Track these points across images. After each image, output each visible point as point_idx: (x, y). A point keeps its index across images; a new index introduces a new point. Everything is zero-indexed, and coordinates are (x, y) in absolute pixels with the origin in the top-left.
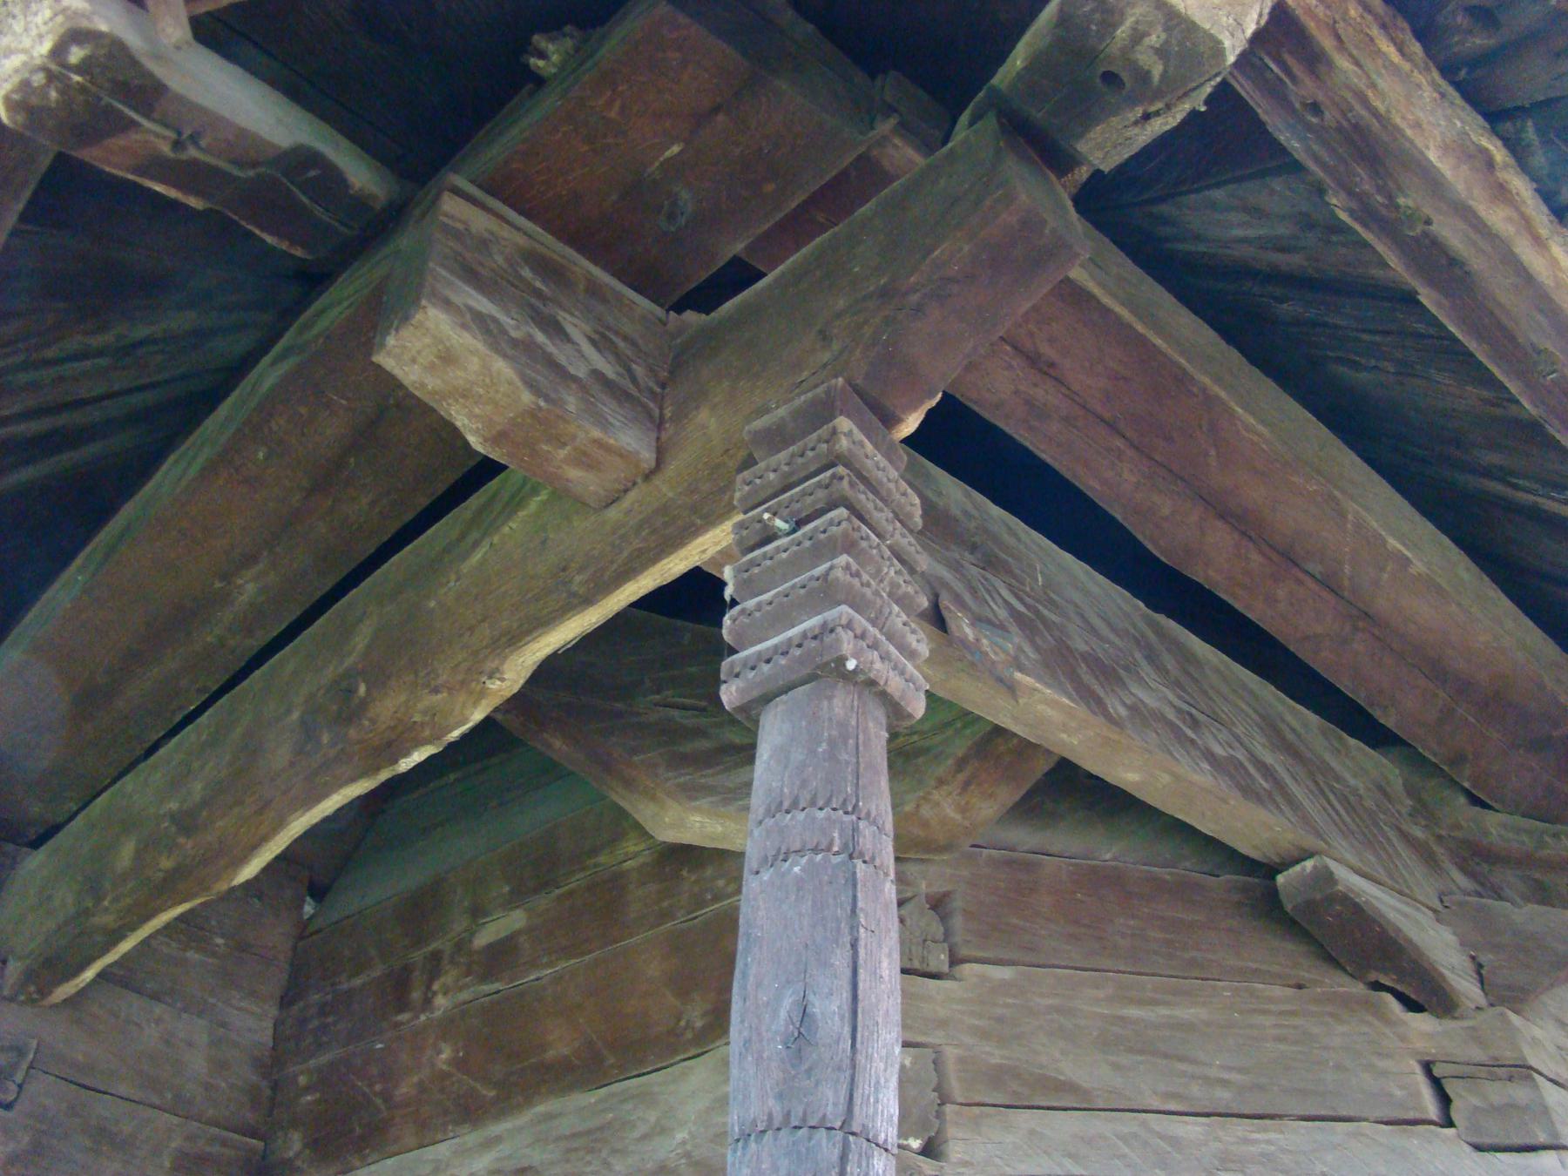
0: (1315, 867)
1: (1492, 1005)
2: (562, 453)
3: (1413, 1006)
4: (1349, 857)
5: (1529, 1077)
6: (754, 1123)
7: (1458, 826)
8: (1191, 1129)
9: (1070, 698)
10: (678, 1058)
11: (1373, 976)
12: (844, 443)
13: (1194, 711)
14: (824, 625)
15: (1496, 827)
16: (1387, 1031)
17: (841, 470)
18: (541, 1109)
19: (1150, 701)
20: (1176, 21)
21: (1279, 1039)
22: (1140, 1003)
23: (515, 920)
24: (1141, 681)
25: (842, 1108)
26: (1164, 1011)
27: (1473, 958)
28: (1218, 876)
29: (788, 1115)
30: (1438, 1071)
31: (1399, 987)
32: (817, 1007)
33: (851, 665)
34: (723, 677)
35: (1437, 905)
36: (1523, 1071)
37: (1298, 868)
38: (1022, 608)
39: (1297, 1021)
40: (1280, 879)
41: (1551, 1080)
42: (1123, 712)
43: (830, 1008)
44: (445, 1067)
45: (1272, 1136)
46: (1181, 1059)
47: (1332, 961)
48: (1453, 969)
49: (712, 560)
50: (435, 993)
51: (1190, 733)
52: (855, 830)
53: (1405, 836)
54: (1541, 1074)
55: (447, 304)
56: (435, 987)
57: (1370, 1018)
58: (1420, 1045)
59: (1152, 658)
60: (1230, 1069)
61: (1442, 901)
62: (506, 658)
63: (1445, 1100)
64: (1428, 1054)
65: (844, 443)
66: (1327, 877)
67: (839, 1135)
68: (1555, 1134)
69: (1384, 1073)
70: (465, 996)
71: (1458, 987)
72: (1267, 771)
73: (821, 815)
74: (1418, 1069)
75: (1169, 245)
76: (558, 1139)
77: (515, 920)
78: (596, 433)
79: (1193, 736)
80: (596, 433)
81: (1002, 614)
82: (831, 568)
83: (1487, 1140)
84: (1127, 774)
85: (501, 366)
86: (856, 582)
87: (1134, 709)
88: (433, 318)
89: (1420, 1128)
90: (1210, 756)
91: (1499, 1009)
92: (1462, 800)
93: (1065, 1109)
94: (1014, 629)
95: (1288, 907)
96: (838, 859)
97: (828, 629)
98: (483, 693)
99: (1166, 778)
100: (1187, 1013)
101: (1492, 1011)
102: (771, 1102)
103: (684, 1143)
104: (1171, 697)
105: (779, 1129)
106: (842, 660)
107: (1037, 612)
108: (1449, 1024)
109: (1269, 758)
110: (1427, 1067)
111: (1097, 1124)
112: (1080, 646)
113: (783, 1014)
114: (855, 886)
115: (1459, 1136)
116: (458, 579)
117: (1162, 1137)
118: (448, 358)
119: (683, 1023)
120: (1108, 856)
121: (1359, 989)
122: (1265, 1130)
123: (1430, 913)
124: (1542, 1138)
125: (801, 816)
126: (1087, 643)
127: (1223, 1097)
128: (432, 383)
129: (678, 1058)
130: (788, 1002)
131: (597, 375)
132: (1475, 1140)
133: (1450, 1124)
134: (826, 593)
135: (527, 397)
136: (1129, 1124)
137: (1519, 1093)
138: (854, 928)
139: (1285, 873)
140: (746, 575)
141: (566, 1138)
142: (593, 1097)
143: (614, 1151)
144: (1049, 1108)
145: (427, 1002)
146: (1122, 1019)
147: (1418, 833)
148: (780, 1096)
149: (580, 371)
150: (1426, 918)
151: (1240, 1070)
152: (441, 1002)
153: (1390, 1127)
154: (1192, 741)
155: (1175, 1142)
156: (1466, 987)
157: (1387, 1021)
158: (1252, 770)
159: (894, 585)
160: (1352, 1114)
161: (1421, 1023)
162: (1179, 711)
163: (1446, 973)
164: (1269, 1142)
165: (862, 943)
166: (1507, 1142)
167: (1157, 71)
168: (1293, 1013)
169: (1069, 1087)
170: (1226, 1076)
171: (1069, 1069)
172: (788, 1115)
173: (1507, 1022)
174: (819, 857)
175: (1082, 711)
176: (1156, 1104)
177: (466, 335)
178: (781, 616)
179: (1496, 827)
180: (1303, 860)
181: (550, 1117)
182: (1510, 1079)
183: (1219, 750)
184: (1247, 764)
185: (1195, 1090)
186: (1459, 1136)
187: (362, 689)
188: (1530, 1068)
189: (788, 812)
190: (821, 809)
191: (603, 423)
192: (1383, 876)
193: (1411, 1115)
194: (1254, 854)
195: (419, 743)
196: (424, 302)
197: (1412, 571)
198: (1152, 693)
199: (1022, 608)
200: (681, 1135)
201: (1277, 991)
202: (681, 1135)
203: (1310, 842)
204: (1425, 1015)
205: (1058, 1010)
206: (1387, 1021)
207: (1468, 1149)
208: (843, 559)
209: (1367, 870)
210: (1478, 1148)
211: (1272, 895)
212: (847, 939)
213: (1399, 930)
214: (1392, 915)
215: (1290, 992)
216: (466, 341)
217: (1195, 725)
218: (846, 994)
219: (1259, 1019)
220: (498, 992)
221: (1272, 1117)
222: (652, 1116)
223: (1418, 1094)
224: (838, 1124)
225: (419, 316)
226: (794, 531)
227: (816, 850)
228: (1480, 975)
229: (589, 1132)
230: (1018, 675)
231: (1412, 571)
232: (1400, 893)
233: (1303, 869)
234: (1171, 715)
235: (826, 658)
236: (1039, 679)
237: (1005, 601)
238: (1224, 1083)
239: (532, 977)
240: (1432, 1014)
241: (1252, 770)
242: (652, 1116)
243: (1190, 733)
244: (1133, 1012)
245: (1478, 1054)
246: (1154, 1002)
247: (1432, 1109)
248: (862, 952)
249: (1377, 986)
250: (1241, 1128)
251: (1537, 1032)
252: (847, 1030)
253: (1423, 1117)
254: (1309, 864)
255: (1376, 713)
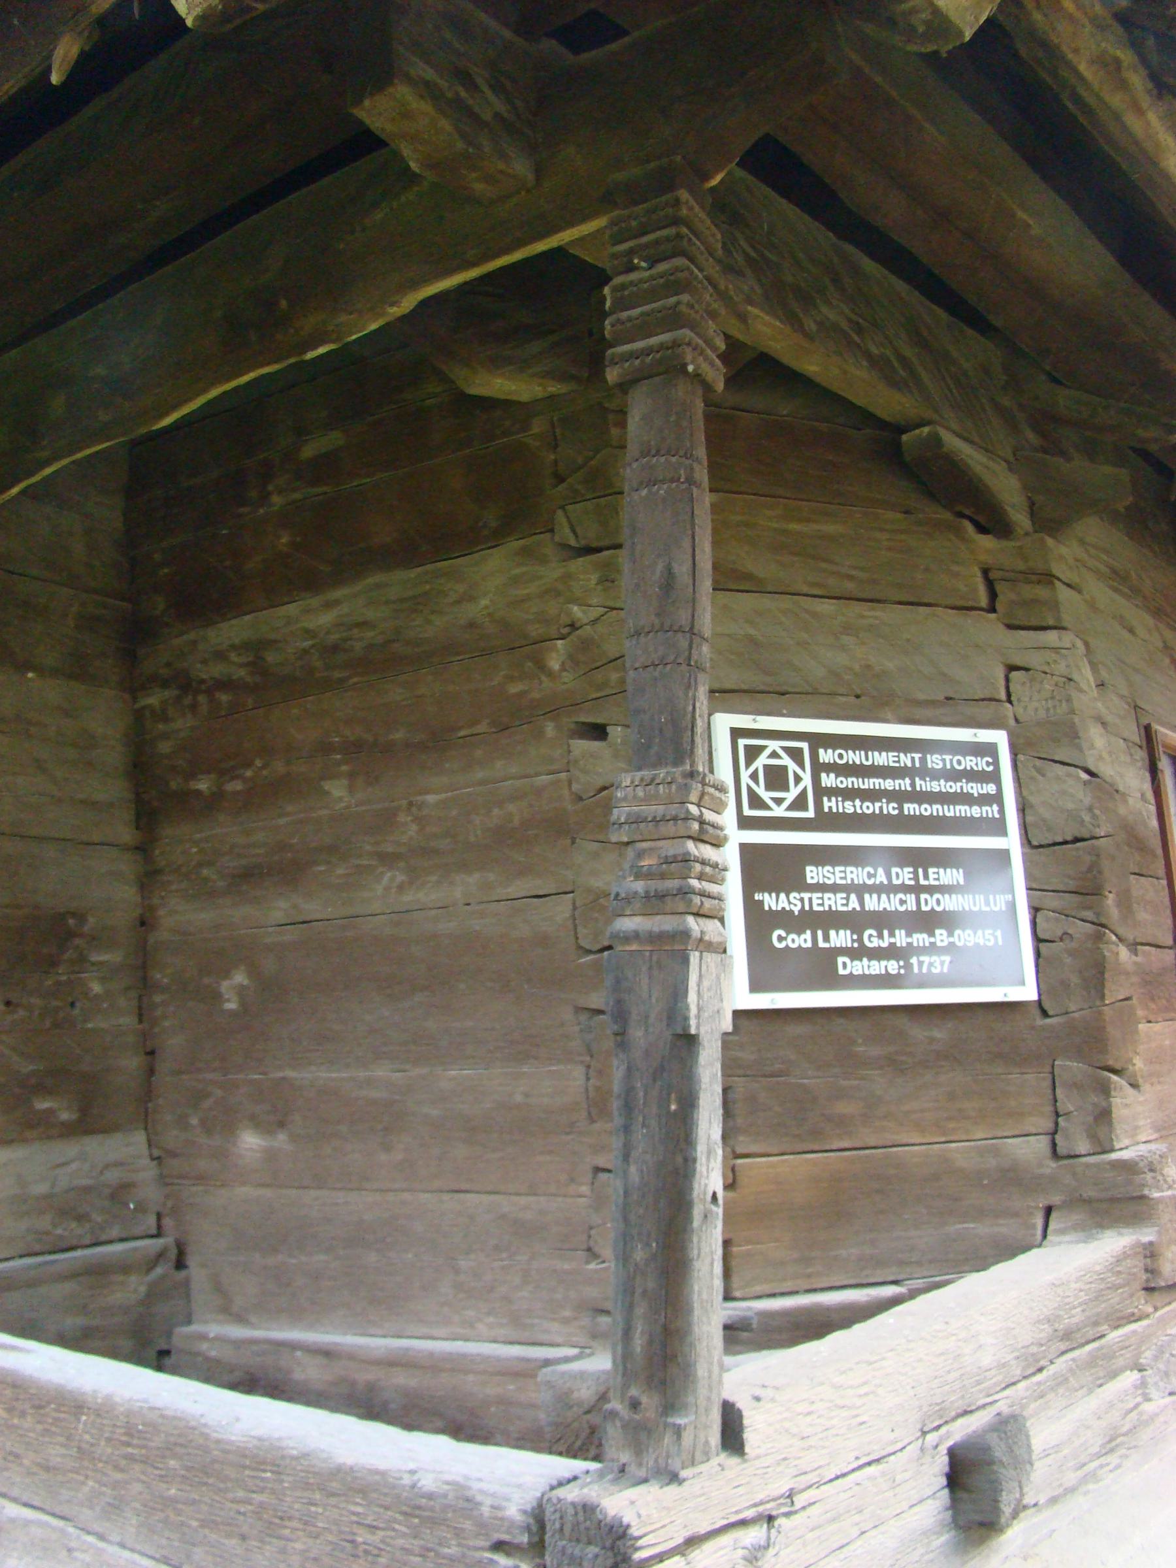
0: (929, 433)
1: (1036, 532)
2: (474, 175)
3: (982, 529)
4: (954, 426)
5: (1052, 583)
6: (643, 628)
7: (1037, 398)
8: (826, 607)
9: (781, 322)
10: (479, 548)
11: (959, 508)
12: (684, 212)
13: (861, 321)
14: (674, 341)
15: (1064, 399)
16: (963, 547)
17: (685, 230)
18: (370, 581)
19: (832, 316)
20: (936, 11)
21: (889, 549)
22: (800, 520)
23: (334, 439)
24: (828, 303)
25: (689, 621)
26: (815, 527)
27: (1029, 498)
28: (859, 429)
29: (662, 624)
30: (992, 575)
31: (976, 517)
32: (676, 568)
33: (690, 368)
34: (607, 363)
35: (1011, 459)
36: (1048, 578)
37: (917, 431)
38: (753, 254)
39: (903, 537)
40: (905, 437)
41: (1065, 583)
42: (814, 327)
43: (682, 570)
44: (285, 549)
45: (878, 614)
46: (824, 560)
47: (931, 496)
48: (1013, 506)
49: (567, 244)
50: (270, 493)
51: (856, 338)
52: (692, 469)
53: (998, 407)
54: (1059, 579)
55: (409, 80)
56: (270, 488)
57: (952, 537)
58: (983, 557)
59: (836, 281)
60: (855, 568)
61: (1015, 455)
62: (406, 295)
63: (993, 595)
64: (986, 563)
65: (684, 212)
66: (936, 441)
67: (688, 635)
68: (1059, 619)
69: (956, 575)
70: (297, 496)
71: (1014, 519)
72: (903, 360)
73: (674, 459)
74: (979, 574)
75: (1062, 1225)
76: (387, 602)
77: (334, 439)
78: (501, 166)
79: (859, 342)
80: (501, 166)
81: (740, 259)
82: (678, 303)
83: (1017, 622)
84: (811, 367)
85: (445, 124)
86: (692, 312)
87: (820, 324)
88: (402, 91)
89: (973, 613)
90: (869, 356)
91: (1041, 535)
92: (1043, 377)
93: (747, 592)
94: (748, 272)
95: (908, 459)
96: (684, 486)
97: (676, 344)
98: (383, 314)
99: (836, 371)
100: (831, 528)
101: (1037, 535)
102: (653, 617)
103: (486, 607)
104: (847, 311)
105: (657, 632)
106: (685, 365)
107: (762, 255)
108: (1004, 543)
109: (909, 352)
110: (985, 572)
111: (766, 602)
112: (790, 279)
113: (658, 574)
114: (693, 502)
115: (998, 619)
116: (364, 230)
117: (806, 611)
118: (407, 115)
119: (480, 524)
120: (785, 412)
121: (947, 516)
122: (873, 609)
123: (1003, 463)
124: (1051, 622)
125: (663, 459)
126: (794, 275)
127: (849, 586)
128: (389, 127)
129: (479, 548)
130: (660, 567)
131: (497, 115)
132: (1007, 622)
133: (992, 609)
134: (673, 320)
135: (460, 145)
136: (786, 602)
137: (1041, 592)
138: (693, 525)
139: (908, 434)
140: (619, 294)
141: (394, 602)
142: (413, 573)
143: (433, 612)
144: (738, 591)
145: (264, 498)
146: (785, 532)
147: (1006, 402)
148: (658, 615)
149: (487, 116)
150: (1000, 467)
151: (862, 569)
152: (277, 500)
153: (954, 611)
154: (858, 346)
155: (815, 615)
156: (1020, 519)
157: (964, 540)
158: (896, 364)
159: (708, 305)
160: (932, 601)
161: (987, 542)
162: (850, 320)
163: (1009, 509)
164: (876, 618)
165: (696, 534)
166: (1027, 624)
167: (921, 29)
168: (901, 532)
169: (749, 577)
170: (854, 573)
171: (749, 566)
172: (662, 624)
173: (1043, 541)
174: (674, 485)
175: (788, 330)
176: (805, 589)
177: (422, 102)
178: (644, 328)
179: (1064, 399)
180: (924, 425)
181: (378, 586)
182: (1039, 582)
183: (875, 350)
184: (892, 358)
185: (832, 581)
186: (998, 619)
187: (284, 304)
188: (1054, 576)
189: (654, 456)
190: (673, 456)
191: (503, 156)
192: (977, 439)
193: (970, 604)
194: (888, 419)
195: (323, 342)
196: (396, 81)
197: (1033, 232)
198: (834, 312)
199: (753, 254)
200: (484, 602)
201: (890, 515)
202: (484, 602)
203: (928, 414)
204: (990, 537)
205: (747, 525)
206: (964, 540)
207: (1002, 627)
208: (685, 298)
209: (965, 434)
210: (1010, 627)
211: (898, 445)
212: (690, 532)
213: (981, 480)
214: (978, 469)
215: (899, 516)
216: (423, 106)
217: (860, 331)
218: (690, 562)
219: (878, 535)
220: (326, 493)
221: (878, 601)
222: (461, 588)
223: (975, 590)
224: (687, 629)
225: (391, 90)
226: (650, 268)
227: (672, 481)
228: (1032, 510)
229: (415, 597)
230: (749, 308)
231: (1033, 232)
232: (987, 450)
233: (922, 432)
234: (844, 325)
235: (675, 363)
236: (762, 309)
237: (744, 251)
238: (850, 578)
239: (355, 484)
240: (995, 536)
241: (896, 364)
242: (461, 588)
243: (856, 338)
244: (794, 526)
245: (1021, 566)
246: (808, 520)
247: (983, 600)
248: (697, 538)
249: (961, 515)
250: (857, 608)
251: (1063, 550)
252: (691, 582)
253: (976, 605)
254: (926, 430)
255: (990, 317)
